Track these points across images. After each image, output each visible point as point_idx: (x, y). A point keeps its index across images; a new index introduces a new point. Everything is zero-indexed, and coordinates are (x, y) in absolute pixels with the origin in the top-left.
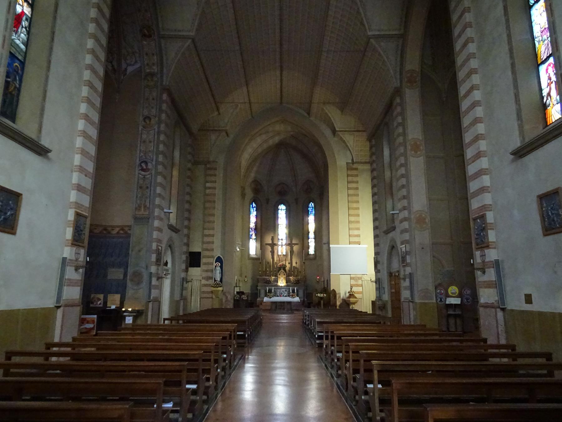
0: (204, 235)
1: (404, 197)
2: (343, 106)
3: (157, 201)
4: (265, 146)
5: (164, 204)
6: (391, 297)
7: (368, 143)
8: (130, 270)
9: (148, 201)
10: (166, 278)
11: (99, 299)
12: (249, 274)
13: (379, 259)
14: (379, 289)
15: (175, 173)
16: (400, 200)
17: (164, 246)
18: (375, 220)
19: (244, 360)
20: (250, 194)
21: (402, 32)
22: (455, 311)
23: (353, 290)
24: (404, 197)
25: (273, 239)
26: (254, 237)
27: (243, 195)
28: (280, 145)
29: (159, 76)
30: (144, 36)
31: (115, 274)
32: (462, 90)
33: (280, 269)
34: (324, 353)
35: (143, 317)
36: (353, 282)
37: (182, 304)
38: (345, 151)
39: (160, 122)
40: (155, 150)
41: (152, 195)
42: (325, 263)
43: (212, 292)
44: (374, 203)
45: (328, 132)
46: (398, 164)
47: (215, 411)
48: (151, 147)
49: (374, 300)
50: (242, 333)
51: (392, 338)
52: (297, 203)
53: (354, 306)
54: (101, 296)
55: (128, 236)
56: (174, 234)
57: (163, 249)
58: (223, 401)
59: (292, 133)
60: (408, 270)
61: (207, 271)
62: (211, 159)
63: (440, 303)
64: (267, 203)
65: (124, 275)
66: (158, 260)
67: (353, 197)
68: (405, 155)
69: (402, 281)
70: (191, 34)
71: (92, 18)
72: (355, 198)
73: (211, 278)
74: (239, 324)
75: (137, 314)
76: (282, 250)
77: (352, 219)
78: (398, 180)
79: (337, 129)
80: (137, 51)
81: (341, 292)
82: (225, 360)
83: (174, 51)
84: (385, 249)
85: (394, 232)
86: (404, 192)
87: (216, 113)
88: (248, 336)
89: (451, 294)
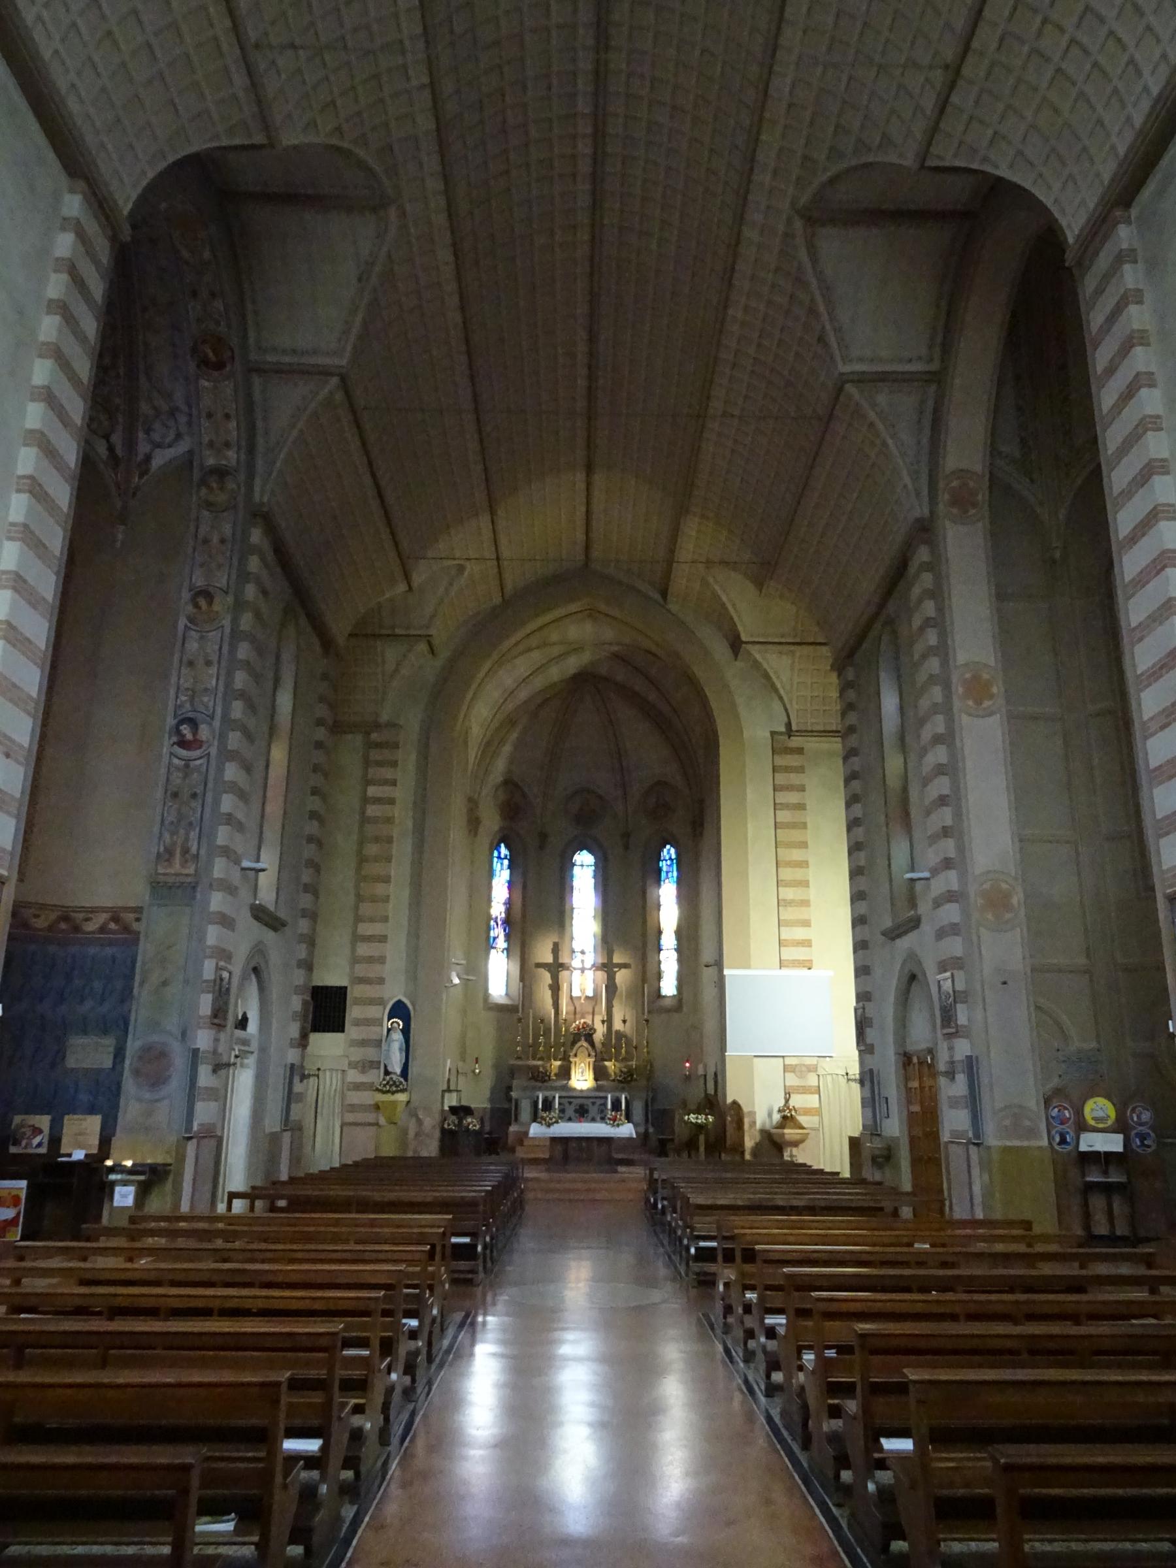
0: (356, 938)
1: (946, 832)
2: (764, 571)
3: (223, 836)
4: (539, 683)
5: (240, 844)
6: (910, 1127)
7: (834, 678)
8: (133, 1046)
9: (194, 835)
10: (242, 1066)
11: (37, 1131)
12: (488, 1052)
13: (870, 1013)
14: (873, 1100)
15: (279, 754)
16: (933, 839)
17: (237, 967)
18: (857, 897)
19: (469, 1325)
20: (491, 821)
21: (935, 366)
22: (1106, 1173)
23: (791, 1103)
24: (946, 832)
25: (556, 950)
26: (501, 943)
27: (474, 823)
28: (583, 680)
29: (242, 477)
30: (204, 363)
31: (88, 1053)
32: (1124, 521)
33: (576, 1038)
34: (719, 1306)
35: (169, 1186)
36: (792, 1080)
37: (287, 1138)
38: (765, 698)
39: (240, 605)
40: (221, 688)
41: (207, 815)
42: (710, 1026)
43: (377, 1107)
44: (854, 848)
45: (720, 650)
46: (927, 734)
47: (378, 1527)
48: (211, 678)
49: (856, 1134)
50: (467, 1240)
51: (949, 1272)
52: (626, 847)
53: (795, 1151)
55: (131, 938)
56: (269, 936)
57: (235, 981)
58: (405, 1485)
59: (615, 648)
60: (963, 1048)
61: (363, 1043)
62: (384, 717)
63: (1057, 1147)
64: (542, 847)
65: (115, 1057)
66: (219, 1015)
67: (789, 829)
68: (946, 708)
69: (943, 1081)
70: (336, 361)
71: (50, 301)
72: (795, 835)
73: (374, 1065)
74: (454, 1210)
75: (151, 1178)
76: (583, 981)
77: (788, 893)
78: (926, 782)
79: (744, 638)
80: (184, 408)
81: (757, 1109)
82: (413, 1334)
83: (288, 408)
84: (889, 985)
85: (916, 932)
86: (945, 816)
87: (402, 587)
88: (485, 1247)
89: (1092, 1123)
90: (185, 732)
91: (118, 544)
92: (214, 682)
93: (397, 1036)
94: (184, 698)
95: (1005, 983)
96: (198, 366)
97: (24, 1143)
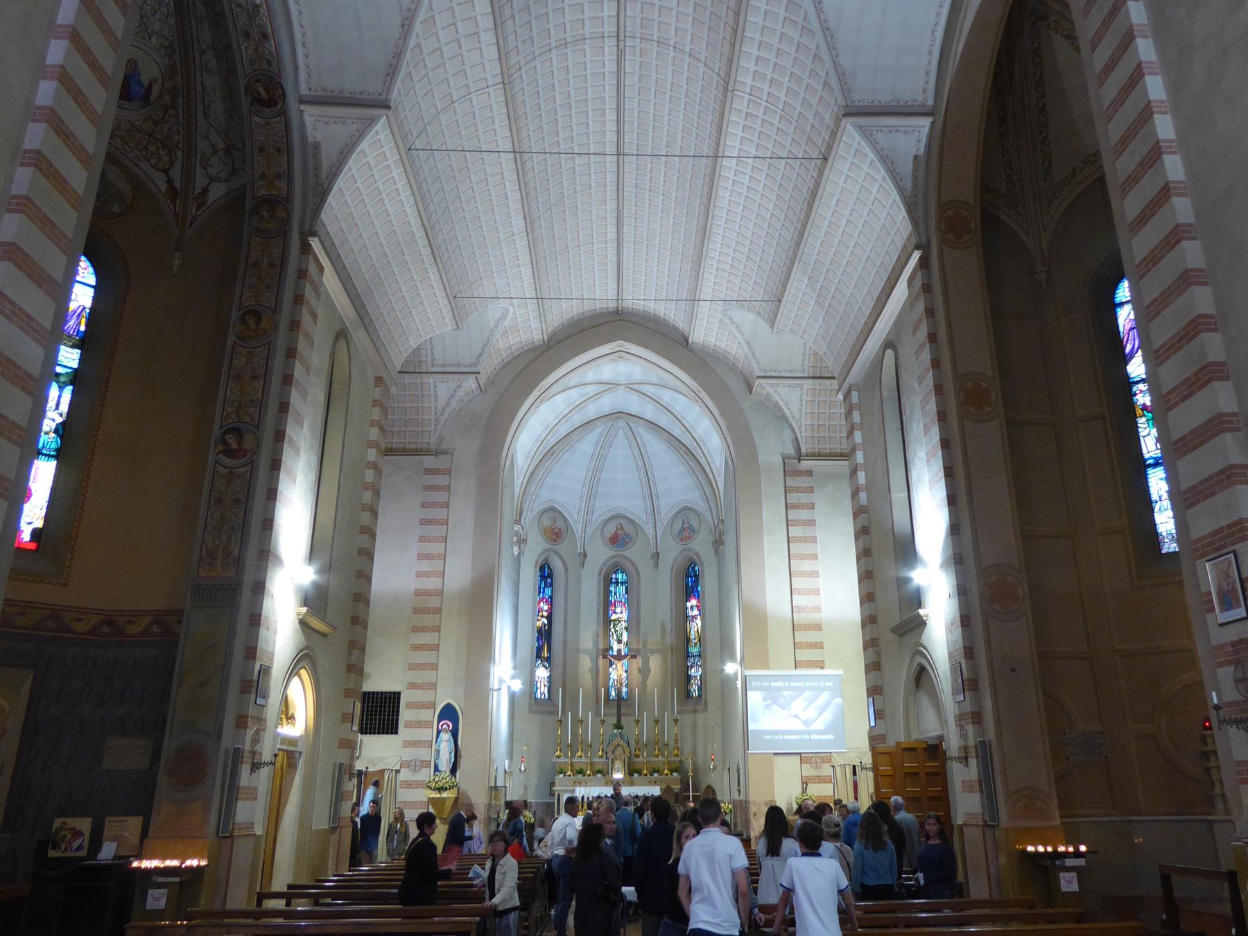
8: (169, 745)
11: (77, 834)
30: (257, 100)
36: (809, 771)
54: (84, 825)
90: (230, 441)
91: (175, 270)
92: (260, 395)
93: (446, 737)
94: (230, 410)
95: (1013, 670)
96: (251, 104)
97: (63, 847)
